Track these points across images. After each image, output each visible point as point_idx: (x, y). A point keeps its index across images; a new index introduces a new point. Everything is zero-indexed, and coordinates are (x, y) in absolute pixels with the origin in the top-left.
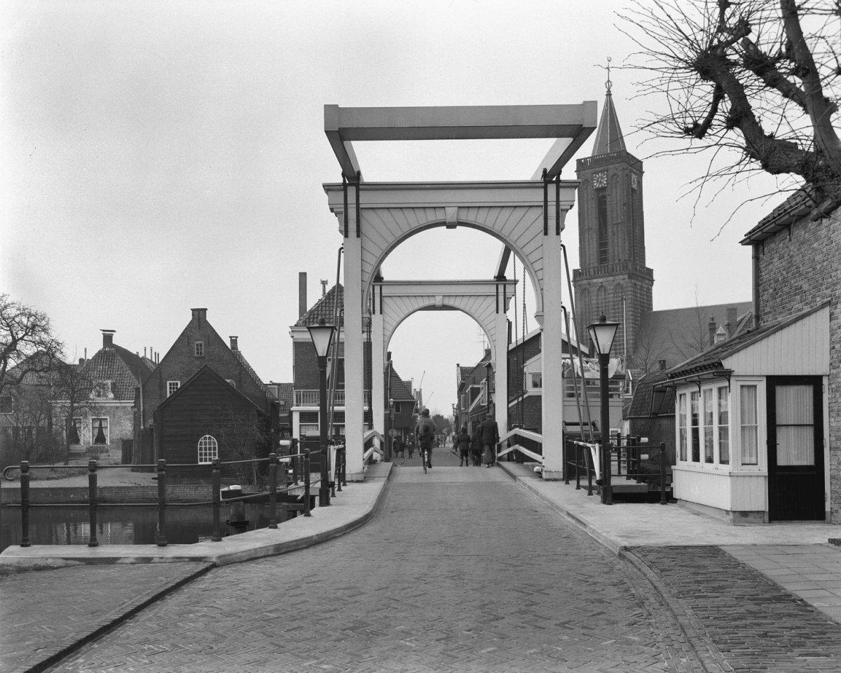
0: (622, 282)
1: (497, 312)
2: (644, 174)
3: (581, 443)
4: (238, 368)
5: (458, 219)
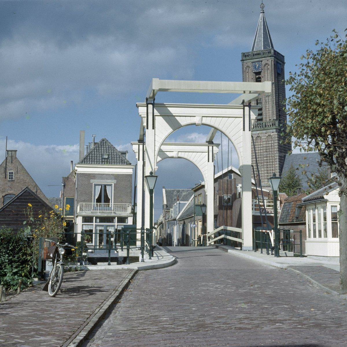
0: (272, 134)
3: (264, 231)
4: (35, 188)
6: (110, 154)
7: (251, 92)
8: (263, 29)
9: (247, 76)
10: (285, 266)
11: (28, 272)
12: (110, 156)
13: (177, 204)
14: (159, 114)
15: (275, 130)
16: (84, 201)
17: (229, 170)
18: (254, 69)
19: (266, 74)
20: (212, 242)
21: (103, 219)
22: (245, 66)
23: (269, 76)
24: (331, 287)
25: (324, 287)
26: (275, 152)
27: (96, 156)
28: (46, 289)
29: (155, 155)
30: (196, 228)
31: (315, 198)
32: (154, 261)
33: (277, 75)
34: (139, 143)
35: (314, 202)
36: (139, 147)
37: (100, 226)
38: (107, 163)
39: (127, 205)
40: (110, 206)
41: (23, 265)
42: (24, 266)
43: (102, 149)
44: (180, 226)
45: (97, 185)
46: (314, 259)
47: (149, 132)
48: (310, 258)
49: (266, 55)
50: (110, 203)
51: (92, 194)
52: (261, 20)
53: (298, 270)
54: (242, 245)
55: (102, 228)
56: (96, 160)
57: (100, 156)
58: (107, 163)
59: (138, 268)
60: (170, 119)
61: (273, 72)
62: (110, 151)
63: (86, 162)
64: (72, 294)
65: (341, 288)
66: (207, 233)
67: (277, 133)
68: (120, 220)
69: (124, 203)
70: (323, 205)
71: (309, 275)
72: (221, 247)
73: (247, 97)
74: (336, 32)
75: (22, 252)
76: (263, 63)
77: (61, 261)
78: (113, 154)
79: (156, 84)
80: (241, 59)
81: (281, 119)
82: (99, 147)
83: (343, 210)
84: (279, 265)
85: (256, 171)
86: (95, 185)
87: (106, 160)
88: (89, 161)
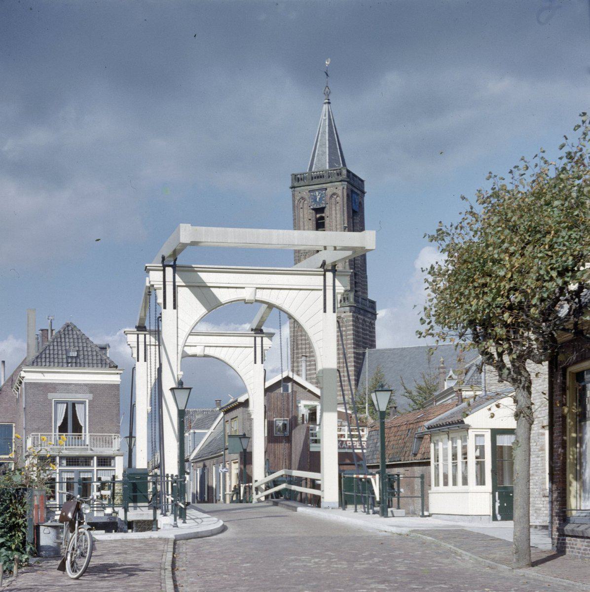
1: (255, 363)
2: (365, 194)
5: (255, 297)
6: (81, 349)
7: (337, 248)
8: (329, 133)
9: (301, 215)
10: (404, 531)
11: (21, 543)
12: (81, 353)
13: (190, 434)
14: (183, 284)
15: (348, 309)
16: (38, 430)
17: (284, 376)
18: (312, 202)
19: (334, 212)
20: (261, 496)
21: (72, 461)
22: (298, 198)
23: (338, 216)
24: (493, 560)
25: (484, 560)
26: (349, 346)
27: (56, 352)
28: (62, 568)
29: (178, 353)
30: (227, 474)
31: (448, 423)
32: (187, 527)
33: (351, 212)
34: (138, 331)
35: (447, 430)
36: (138, 338)
37: (68, 471)
38: (76, 366)
39: (113, 437)
40: (83, 439)
41: (11, 532)
42: (13, 533)
43: (67, 340)
44: (197, 471)
45: (59, 403)
46: (445, 520)
47: (168, 314)
48: (436, 518)
49: (334, 179)
50: (83, 434)
51: (51, 418)
52: (325, 116)
53: (431, 536)
54: (322, 499)
55: (72, 475)
56: (56, 360)
57: (64, 352)
58: (76, 366)
59: (175, 536)
60: (201, 291)
61: (345, 208)
62: (81, 344)
63: (40, 363)
64: (102, 575)
65: (515, 560)
66: (253, 481)
67: (351, 314)
68: (102, 462)
69: (106, 432)
70: (463, 434)
71: (450, 543)
72: (282, 504)
73: (330, 257)
74: (525, 162)
75: (10, 512)
76: (329, 192)
77: (84, 524)
78: (85, 349)
79: (186, 233)
80: (290, 185)
81: (358, 289)
82: (61, 338)
83: (520, 441)
84: (394, 530)
85: (344, 381)
86: (57, 403)
87: (74, 361)
88: (45, 361)
